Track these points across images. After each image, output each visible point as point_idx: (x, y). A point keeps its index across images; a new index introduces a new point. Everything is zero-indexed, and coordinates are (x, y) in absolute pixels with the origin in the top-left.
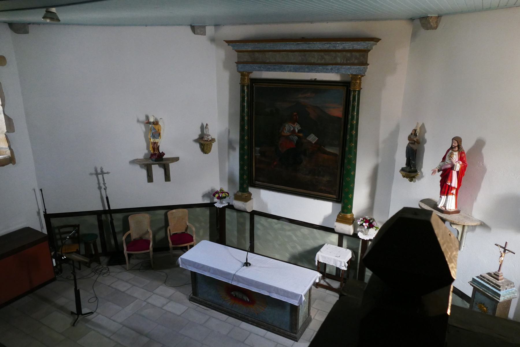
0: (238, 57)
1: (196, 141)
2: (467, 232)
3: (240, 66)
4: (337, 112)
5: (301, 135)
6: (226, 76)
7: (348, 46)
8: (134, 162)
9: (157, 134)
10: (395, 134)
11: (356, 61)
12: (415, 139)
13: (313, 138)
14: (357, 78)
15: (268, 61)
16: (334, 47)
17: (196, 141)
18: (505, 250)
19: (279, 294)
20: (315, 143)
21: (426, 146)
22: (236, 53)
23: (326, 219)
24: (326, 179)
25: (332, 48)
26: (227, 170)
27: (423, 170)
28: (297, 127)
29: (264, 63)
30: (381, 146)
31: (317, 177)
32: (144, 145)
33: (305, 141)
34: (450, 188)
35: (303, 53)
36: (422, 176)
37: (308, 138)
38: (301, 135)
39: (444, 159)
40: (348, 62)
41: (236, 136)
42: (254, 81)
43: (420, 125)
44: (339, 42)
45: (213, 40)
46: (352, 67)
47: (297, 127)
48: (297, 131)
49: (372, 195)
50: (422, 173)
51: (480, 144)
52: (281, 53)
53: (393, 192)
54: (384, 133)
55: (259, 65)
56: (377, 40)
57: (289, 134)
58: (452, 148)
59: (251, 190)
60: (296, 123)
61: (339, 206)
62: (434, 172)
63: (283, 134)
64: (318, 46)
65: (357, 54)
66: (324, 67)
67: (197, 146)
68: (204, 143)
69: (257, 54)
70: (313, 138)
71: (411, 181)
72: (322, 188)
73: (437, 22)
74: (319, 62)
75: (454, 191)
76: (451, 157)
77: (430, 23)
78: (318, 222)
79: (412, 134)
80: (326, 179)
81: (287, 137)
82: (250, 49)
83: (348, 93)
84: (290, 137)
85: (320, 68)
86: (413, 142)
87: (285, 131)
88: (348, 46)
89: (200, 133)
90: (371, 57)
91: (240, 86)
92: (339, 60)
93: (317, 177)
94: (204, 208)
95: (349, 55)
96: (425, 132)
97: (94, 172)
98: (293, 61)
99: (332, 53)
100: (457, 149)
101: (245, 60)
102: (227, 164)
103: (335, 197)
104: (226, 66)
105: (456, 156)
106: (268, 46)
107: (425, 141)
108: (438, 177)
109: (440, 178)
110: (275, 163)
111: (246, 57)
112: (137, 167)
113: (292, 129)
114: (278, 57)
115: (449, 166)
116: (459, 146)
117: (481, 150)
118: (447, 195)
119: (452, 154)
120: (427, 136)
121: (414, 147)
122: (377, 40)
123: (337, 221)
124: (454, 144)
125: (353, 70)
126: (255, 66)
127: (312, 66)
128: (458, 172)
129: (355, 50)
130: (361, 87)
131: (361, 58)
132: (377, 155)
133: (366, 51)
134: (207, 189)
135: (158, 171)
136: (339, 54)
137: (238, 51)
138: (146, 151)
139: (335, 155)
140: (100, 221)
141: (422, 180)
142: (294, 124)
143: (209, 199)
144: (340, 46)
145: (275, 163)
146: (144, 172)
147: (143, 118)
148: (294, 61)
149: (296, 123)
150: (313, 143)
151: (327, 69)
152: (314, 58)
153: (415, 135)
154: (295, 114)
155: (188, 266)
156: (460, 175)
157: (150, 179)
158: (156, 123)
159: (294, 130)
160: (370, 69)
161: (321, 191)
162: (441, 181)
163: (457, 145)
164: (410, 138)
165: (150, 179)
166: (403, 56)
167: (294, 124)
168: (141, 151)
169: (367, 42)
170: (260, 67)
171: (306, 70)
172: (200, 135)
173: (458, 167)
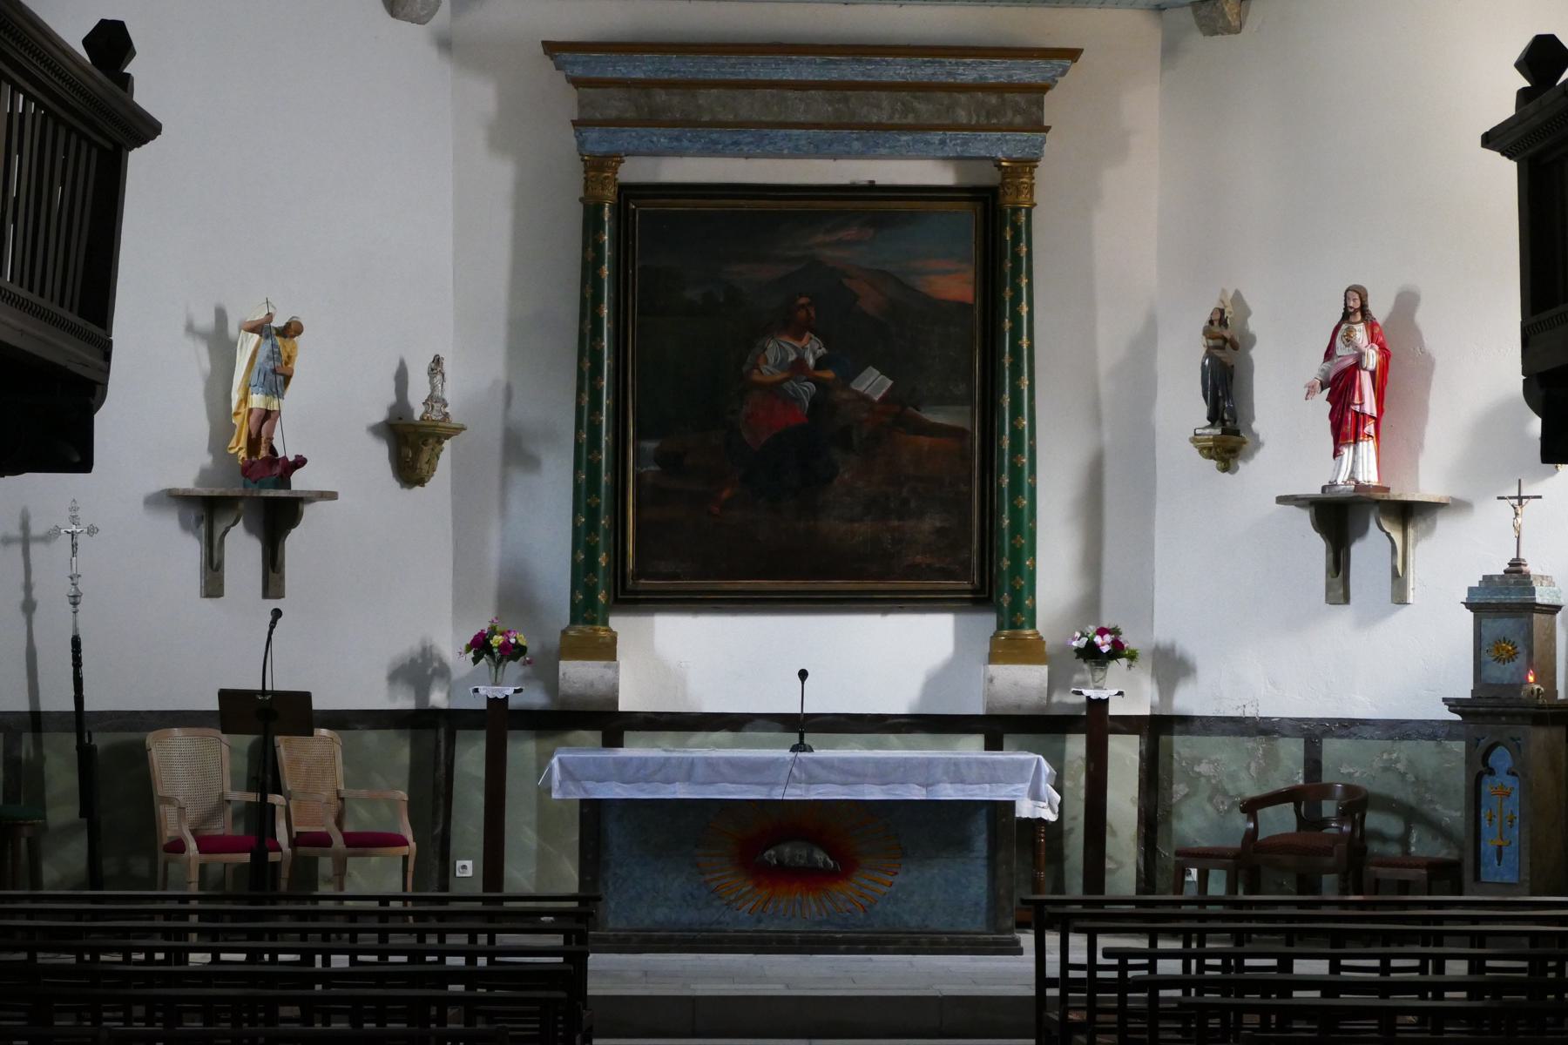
0: (582, 106)
1: (378, 430)
2: (1415, 545)
3: (593, 134)
4: (955, 284)
5: (828, 374)
6: (501, 175)
7: (993, 72)
9: (278, 377)
10: (1143, 348)
11: (1018, 120)
12: (1227, 334)
14: (1027, 165)
15: (706, 118)
16: (949, 74)
17: (378, 430)
18: (1520, 498)
19: (962, 782)
20: (882, 399)
21: (1255, 353)
22: (572, 93)
23: (935, 681)
24: (931, 523)
25: (943, 79)
26: (494, 554)
27: (1255, 426)
28: (812, 350)
30: (1106, 388)
31: (896, 523)
32: (199, 427)
33: (845, 395)
34: (1360, 418)
35: (838, 94)
36: (1258, 445)
37: (853, 386)
38: (828, 374)
39: (1329, 354)
40: (994, 121)
41: (554, 408)
42: (629, 192)
43: (1230, 294)
44: (968, 61)
45: (445, 44)
46: (1009, 136)
47: (812, 350)
48: (811, 362)
49: (1092, 563)
50: (1256, 436)
51: (1407, 303)
52: (759, 92)
53: (1158, 522)
54: (1110, 347)
55: (676, 131)
56: (1073, 54)
57: (779, 376)
58: (1346, 316)
60: (808, 334)
61: (985, 623)
62: (1310, 391)
63: (756, 377)
64: (897, 70)
65: (1019, 98)
66: (918, 136)
67: (380, 452)
68: (410, 444)
69: (661, 96)
70: (873, 383)
71: (1225, 470)
72: (919, 558)
73: (1239, 14)
74: (896, 120)
75: (1370, 428)
76: (1349, 340)
77: (1224, 15)
78: (899, 704)
79: (1211, 322)
80: (931, 523)
81: (774, 389)
82: (639, 75)
83: (993, 223)
84: (786, 385)
85: (904, 138)
86: (1220, 342)
87: (764, 368)
88: (993, 72)
89: (391, 398)
90: (1054, 107)
91: (578, 210)
92: (962, 116)
93: (896, 523)
94: (391, 734)
95: (993, 99)
96: (1248, 313)
97: (16, 532)
98: (801, 117)
99: (940, 95)
100: (1359, 317)
101: (613, 114)
102: (494, 535)
103: (965, 585)
104: (501, 138)
105: (1360, 334)
106: (712, 69)
107: (1251, 341)
108: (1321, 405)
109: (1329, 406)
110: (725, 494)
112: (169, 524)
113: (792, 357)
114: (747, 106)
115: (1351, 361)
116: (1363, 309)
117: (1412, 320)
118: (1356, 442)
119: (1350, 331)
120: (1253, 325)
121: (1226, 355)
122: (1073, 54)
123: (993, 658)
124: (1351, 304)
125: (1006, 147)
126: (661, 137)
128: (1373, 373)
129: (1008, 91)
130: (1035, 200)
131: (1022, 107)
133: (1039, 90)
135: (242, 549)
136: (963, 98)
137: (576, 82)
138: (207, 460)
139: (959, 433)
141: (1261, 457)
142: (800, 339)
143: (412, 693)
144: (968, 72)
145: (725, 494)
146: (191, 549)
147: (206, 320)
148: (810, 118)
149: (808, 334)
150: (876, 399)
151: (928, 143)
153: (1223, 322)
154: (803, 301)
155: (589, 785)
156: (1380, 380)
158: (291, 330)
159: (800, 362)
160: (1053, 145)
161: (913, 572)
162: (1331, 415)
163: (1357, 304)
164: (1208, 333)
166: (1143, 106)
167: (800, 339)
169: (1055, 62)
170: (678, 139)
171: (856, 145)
172: (392, 409)
173: (1372, 359)
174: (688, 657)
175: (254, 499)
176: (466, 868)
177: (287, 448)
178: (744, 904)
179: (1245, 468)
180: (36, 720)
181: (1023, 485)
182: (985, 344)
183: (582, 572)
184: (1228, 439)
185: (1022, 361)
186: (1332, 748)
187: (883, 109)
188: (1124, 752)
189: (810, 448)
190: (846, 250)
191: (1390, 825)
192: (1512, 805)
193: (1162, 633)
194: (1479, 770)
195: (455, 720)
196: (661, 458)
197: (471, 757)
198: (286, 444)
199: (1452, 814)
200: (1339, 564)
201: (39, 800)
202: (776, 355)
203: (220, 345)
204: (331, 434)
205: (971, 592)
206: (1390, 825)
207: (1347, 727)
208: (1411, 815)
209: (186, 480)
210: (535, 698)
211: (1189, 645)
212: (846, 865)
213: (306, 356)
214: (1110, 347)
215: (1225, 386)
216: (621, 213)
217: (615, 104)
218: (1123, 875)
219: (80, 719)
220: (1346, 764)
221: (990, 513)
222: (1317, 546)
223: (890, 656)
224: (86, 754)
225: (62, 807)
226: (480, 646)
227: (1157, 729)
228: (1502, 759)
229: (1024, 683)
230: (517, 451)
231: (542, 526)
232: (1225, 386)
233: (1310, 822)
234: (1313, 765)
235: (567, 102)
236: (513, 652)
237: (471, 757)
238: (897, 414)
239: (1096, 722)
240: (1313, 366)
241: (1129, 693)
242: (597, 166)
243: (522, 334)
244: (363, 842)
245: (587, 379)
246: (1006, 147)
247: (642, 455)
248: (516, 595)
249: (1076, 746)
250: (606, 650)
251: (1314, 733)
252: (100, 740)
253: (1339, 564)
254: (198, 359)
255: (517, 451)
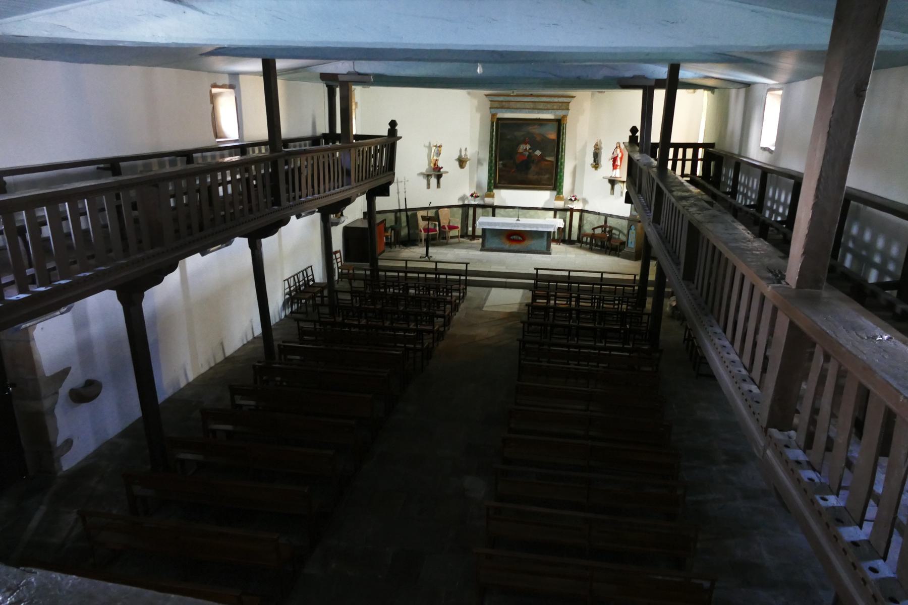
4: (553, 136)
6: (478, 116)
7: (561, 100)
8: (422, 174)
9: (438, 154)
13: (538, 153)
14: (565, 117)
23: (546, 203)
24: (547, 176)
26: (475, 180)
28: (528, 147)
29: (508, 108)
41: (485, 156)
42: (498, 119)
47: (528, 147)
54: (579, 147)
59: (495, 191)
61: (555, 193)
67: (457, 163)
68: (462, 162)
80: (547, 176)
83: (559, 124)
88: (561, 100)
104: (478, 109)
105: (618, 151)
108: (611, 162)
111: (496, 105)
112: (421, 178)
114: (518, 105)
120: (603, 146)
126: (504, 110)
127: (540, 110)
132: (576, 159)
134: (461, 194)
135: (433, 181)
140: (396, 218)
144: (556, 100)
146: (425, 181)
147: (427, 144)
152: (506, 105)
157: (429, 186)
158: (440, 146)
165: (429, 186)
168: (424, 167)
173: (620, 156)
174: (506, 196)
175: (436, 173)
176: (470, 229)
177: (440, 166)
178: (507, 245)
179: (599, 170)
180: (400, 211)
181: (562, 171)
182: (557, 147)
183: (489, 183)
184: (596, 164)
185: (563, 150)
186: (609, 219)
187: (541, 106)
188: (576, 215)
189: (527, 163)
190: (535, 130)
191: (617, 233)
192: (634, 235)
193: (584, 195)
194: (629, 229)
195: (469, 206)
196: (504, 165)
197: (471, 211)
198: (440, 165)
199: (625, 232)
200: (613, 188)
201: (400, 224)
202: (522, 148)
203: (430, 148)
204: (447, 162)
205: (468, 283)
206: (617, 233)
207: (611, 216)
208: (620, 232)
209: (424, 171)
210: (481, 203)
211: (588, 198)
212: (524, 240)
213: (443, 150)
214: (579, 147)
215: (596, 156)
216: (497, 123)
217: (496, 105)
218: (574, 236)
219: (406, 210)
220: (611, 222)
221: (556, 175)
222: (609, 186)
223: (541, 197)
224: (407, 216)
225: (404, 224)
226: (472, 195)
227: (582, 211)
228: (633, 227)
229: (560, 204)
230: (479, 162)
231: (483, 174)
232: (596, 156)
233: (604, 231)
234: (606, 222)
235: (488, 104)
236: (476, 197)
237: (471, 211)
238: (542, 158)
239: (572, 210)
240: (611, 156)
241: (577, 206)
242: (493, 115)
243: (481, 143)
244: (452, 228)
245: (491, 151)
246: (560, 113)
247: (500, 164)
248: (479, 186)
249: (568, 213)
250: (493, 196)
251: (607, 216)
252: (409, 213)
253: (613, 188)
254: (426, 150)
255: (479, 162)
